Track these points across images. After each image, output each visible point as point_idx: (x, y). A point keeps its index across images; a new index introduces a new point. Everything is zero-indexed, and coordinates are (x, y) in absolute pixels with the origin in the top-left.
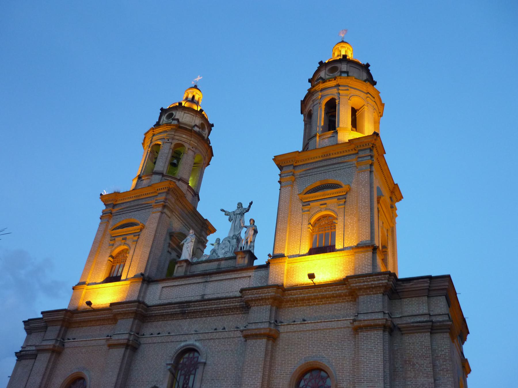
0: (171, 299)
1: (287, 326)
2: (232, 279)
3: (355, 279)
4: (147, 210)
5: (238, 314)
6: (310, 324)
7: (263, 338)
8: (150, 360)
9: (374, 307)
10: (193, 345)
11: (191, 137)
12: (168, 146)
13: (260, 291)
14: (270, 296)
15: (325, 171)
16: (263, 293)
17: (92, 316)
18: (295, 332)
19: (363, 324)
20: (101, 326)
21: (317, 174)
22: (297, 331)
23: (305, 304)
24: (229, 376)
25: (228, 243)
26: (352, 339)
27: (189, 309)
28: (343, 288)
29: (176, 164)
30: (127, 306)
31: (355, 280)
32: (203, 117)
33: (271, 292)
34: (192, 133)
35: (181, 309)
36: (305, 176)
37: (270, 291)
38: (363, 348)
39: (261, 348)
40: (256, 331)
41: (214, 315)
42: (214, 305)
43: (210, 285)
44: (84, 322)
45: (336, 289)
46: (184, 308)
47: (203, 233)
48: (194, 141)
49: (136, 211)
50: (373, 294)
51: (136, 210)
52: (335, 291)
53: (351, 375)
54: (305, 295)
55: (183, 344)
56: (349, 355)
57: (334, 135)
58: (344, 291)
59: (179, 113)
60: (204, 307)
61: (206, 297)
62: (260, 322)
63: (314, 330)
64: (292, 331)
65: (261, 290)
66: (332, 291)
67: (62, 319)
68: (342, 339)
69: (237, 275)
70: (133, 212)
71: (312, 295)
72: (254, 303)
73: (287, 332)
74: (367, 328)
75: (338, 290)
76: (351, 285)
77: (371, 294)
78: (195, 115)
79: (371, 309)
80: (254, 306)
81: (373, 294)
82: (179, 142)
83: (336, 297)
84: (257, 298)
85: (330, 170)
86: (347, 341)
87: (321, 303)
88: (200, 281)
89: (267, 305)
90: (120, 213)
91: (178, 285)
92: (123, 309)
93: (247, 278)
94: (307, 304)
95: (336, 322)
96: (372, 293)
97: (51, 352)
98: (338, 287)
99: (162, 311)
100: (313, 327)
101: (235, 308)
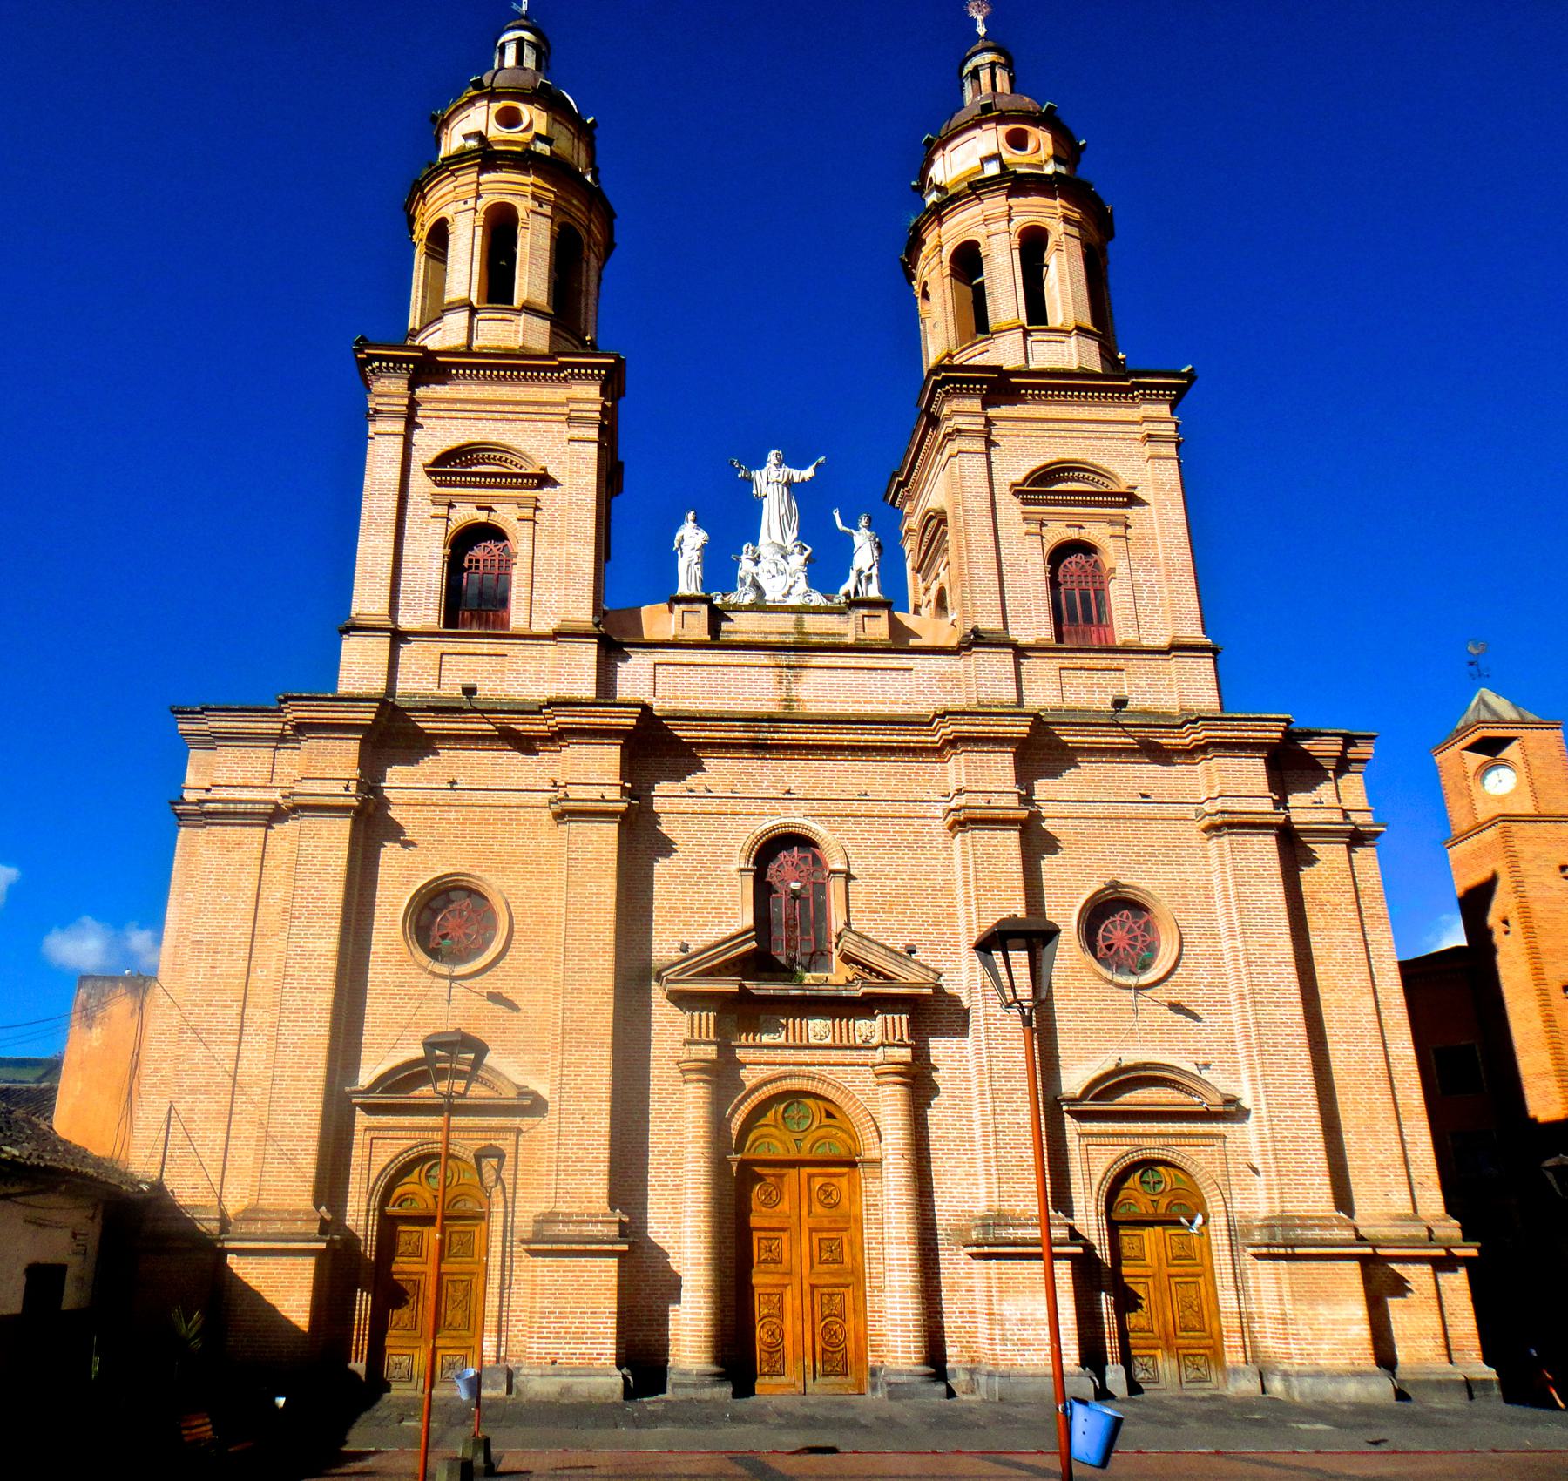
4: (540, 424)
25: (783, 561)
27: (776, 736)
35: (751, 734)
57: (1063, 339)
60: (819, 737)
61: (797, 709)
62: (995, 792)
64: (1059, 815)
90: (441, 414)
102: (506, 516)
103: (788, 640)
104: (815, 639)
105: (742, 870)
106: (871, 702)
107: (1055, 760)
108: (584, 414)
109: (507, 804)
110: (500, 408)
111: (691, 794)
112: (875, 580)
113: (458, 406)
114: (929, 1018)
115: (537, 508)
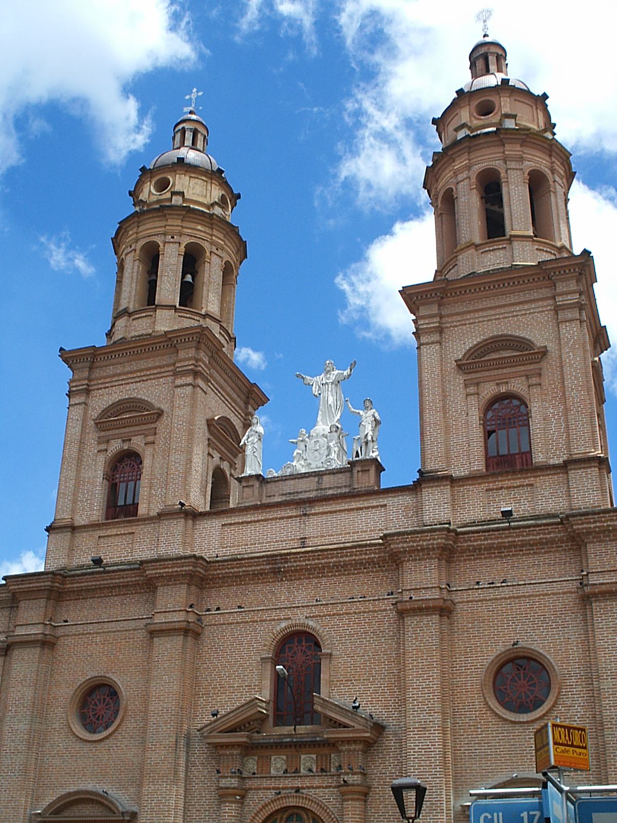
0: (243, 547)
1: (466, 591)
2: (352, 510)
3: (581, 518)
5: (377, 572)
6: (506, 588)
7: (431, 614)
8: (229, 651)
9: (612, 563)
10: (303, 625)
11: (212, 229)
12: (174, 250)
13: (418, 537)
14: (437, 544)
15: (497, 317)
16: (424, 541)
17: (103, 580)
18: (482, 601)
19: (599, 589)
20: (123, 597)
21: (484, 321)
22: (486, 600)
23: (493, 556)
24: (376, 674)
26: (579, 611)
28: (557, 530)
29: (189, 282)
30: (173, 564)
31: (580, 520)
32: (224, 184)
33: (438, 539)
34: (214, 221)
35: (271, 566)
36: (461, 325)
37: (436, 537)
38: (601, 627)
39: (431, 629)
40: (420, 603)
41: (332, 574)
42: (332, 558)
43: (313, 520)
44: (88, 590)
45: (546, 531)
46: (276, 563)
47: (250, 409)
48: (219, 237)
49: (140, 381)
50: (610, 540)
51: (138, 380)
52: (545, 534)
53: (581, 666)
54: (493, 541)
55: (283, 625)
56: (577, 636)
57: (505, 246)
58: (559, 535)
59: (180, 178)
63: (514, 597)
65: (419, 535)
66: (539, 534)
67: (48, 587)
68: (562, 611)
69: (361, 502)
70: (132, 383)
71: (506, 540)
72: (408, 555)
73: (468, 602)
74: (606, 596)
75: (549, 533)
76: (574, 527)
77: (606, 541)
78: (210, 181)
79: (608, 564)
80: (409, 560)
81: (610, 540)
82: (193, 240)
83: (546, 543)
84: (413, 548)
85: (506, 315)
86: (570, 614)
87: (521, 553)
88: (294, 514)
89: (431, 558)
91: (251, 522)
92: (167, 570)
93: (380, 508)
94: (497, 555)
95: (548, 584)
96: (608, 539)
97: (39, 645)
98: (550, 528)
99: (236, 570)
100: (511, 593)
101: (371, 562)
102: (137, 443)
103: (311, 496)
104: (330, 492)
105: (262, 659)
106: (358, 532)
107: (475, 559)
108: (184, 368)
109: (128, 628)
110: (139, 374)
111: (66, 624)
112: (228, 476)
113: (115, 379)
114: (382, 752)
115: (155, 434)
